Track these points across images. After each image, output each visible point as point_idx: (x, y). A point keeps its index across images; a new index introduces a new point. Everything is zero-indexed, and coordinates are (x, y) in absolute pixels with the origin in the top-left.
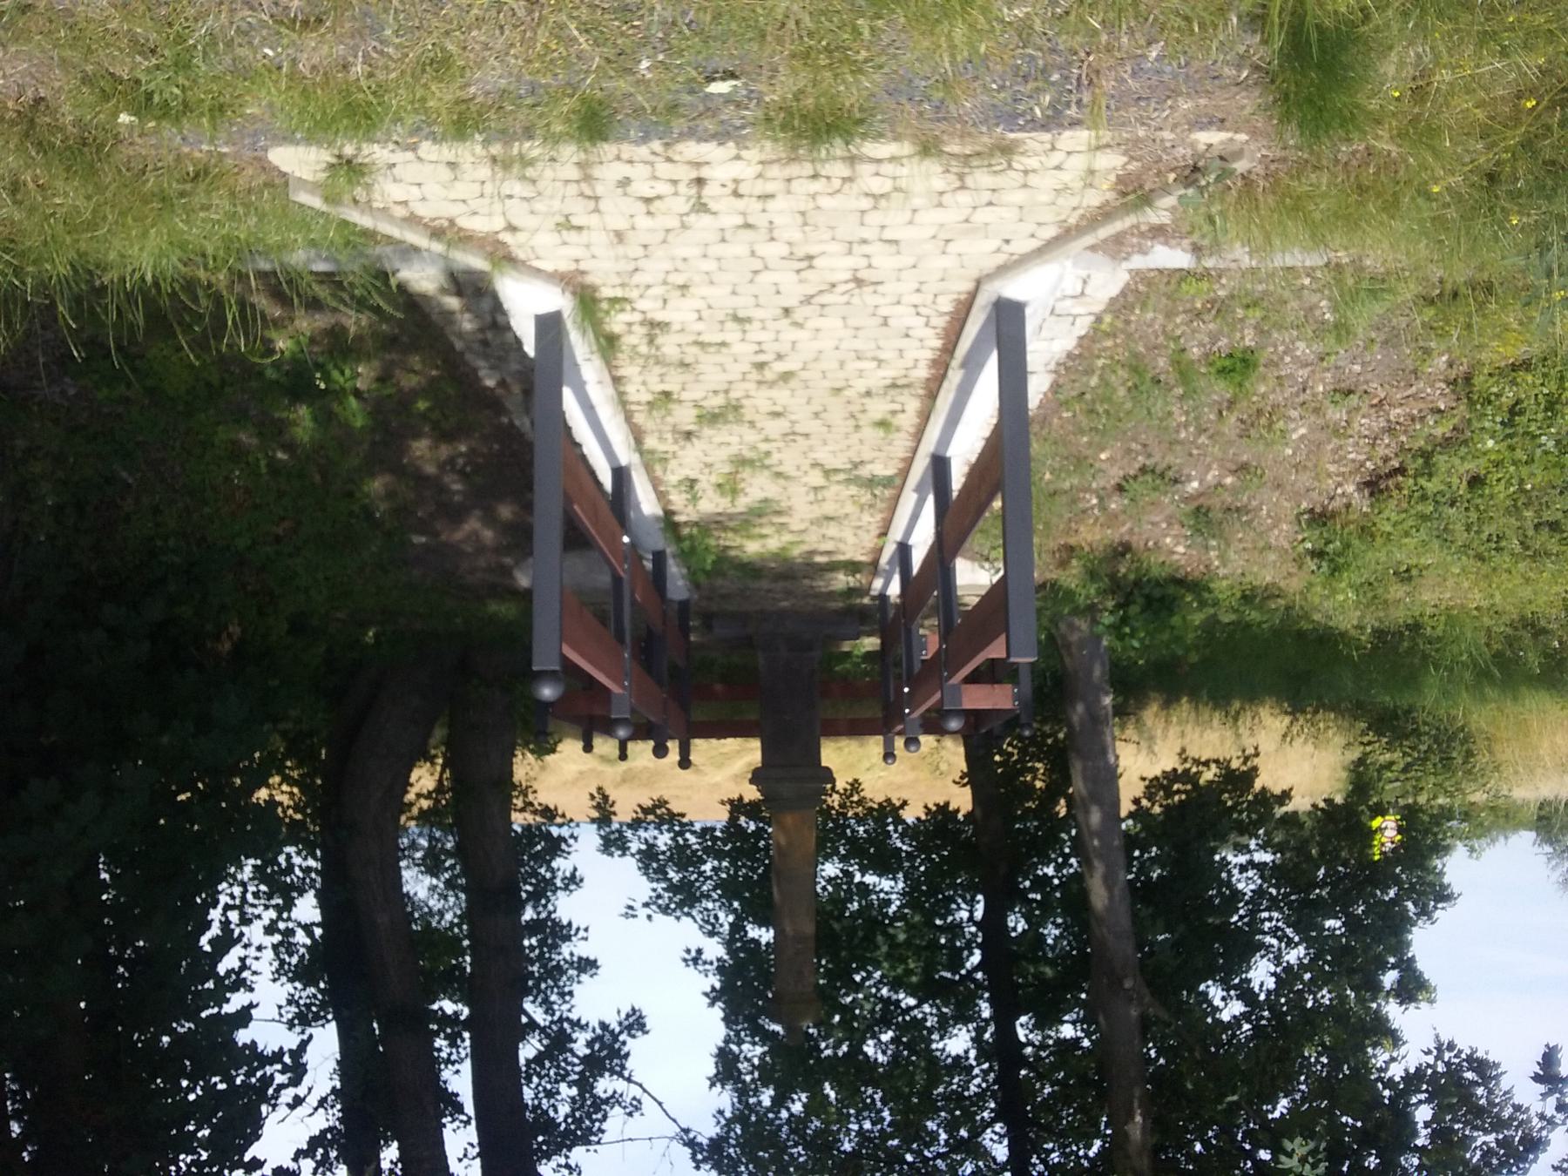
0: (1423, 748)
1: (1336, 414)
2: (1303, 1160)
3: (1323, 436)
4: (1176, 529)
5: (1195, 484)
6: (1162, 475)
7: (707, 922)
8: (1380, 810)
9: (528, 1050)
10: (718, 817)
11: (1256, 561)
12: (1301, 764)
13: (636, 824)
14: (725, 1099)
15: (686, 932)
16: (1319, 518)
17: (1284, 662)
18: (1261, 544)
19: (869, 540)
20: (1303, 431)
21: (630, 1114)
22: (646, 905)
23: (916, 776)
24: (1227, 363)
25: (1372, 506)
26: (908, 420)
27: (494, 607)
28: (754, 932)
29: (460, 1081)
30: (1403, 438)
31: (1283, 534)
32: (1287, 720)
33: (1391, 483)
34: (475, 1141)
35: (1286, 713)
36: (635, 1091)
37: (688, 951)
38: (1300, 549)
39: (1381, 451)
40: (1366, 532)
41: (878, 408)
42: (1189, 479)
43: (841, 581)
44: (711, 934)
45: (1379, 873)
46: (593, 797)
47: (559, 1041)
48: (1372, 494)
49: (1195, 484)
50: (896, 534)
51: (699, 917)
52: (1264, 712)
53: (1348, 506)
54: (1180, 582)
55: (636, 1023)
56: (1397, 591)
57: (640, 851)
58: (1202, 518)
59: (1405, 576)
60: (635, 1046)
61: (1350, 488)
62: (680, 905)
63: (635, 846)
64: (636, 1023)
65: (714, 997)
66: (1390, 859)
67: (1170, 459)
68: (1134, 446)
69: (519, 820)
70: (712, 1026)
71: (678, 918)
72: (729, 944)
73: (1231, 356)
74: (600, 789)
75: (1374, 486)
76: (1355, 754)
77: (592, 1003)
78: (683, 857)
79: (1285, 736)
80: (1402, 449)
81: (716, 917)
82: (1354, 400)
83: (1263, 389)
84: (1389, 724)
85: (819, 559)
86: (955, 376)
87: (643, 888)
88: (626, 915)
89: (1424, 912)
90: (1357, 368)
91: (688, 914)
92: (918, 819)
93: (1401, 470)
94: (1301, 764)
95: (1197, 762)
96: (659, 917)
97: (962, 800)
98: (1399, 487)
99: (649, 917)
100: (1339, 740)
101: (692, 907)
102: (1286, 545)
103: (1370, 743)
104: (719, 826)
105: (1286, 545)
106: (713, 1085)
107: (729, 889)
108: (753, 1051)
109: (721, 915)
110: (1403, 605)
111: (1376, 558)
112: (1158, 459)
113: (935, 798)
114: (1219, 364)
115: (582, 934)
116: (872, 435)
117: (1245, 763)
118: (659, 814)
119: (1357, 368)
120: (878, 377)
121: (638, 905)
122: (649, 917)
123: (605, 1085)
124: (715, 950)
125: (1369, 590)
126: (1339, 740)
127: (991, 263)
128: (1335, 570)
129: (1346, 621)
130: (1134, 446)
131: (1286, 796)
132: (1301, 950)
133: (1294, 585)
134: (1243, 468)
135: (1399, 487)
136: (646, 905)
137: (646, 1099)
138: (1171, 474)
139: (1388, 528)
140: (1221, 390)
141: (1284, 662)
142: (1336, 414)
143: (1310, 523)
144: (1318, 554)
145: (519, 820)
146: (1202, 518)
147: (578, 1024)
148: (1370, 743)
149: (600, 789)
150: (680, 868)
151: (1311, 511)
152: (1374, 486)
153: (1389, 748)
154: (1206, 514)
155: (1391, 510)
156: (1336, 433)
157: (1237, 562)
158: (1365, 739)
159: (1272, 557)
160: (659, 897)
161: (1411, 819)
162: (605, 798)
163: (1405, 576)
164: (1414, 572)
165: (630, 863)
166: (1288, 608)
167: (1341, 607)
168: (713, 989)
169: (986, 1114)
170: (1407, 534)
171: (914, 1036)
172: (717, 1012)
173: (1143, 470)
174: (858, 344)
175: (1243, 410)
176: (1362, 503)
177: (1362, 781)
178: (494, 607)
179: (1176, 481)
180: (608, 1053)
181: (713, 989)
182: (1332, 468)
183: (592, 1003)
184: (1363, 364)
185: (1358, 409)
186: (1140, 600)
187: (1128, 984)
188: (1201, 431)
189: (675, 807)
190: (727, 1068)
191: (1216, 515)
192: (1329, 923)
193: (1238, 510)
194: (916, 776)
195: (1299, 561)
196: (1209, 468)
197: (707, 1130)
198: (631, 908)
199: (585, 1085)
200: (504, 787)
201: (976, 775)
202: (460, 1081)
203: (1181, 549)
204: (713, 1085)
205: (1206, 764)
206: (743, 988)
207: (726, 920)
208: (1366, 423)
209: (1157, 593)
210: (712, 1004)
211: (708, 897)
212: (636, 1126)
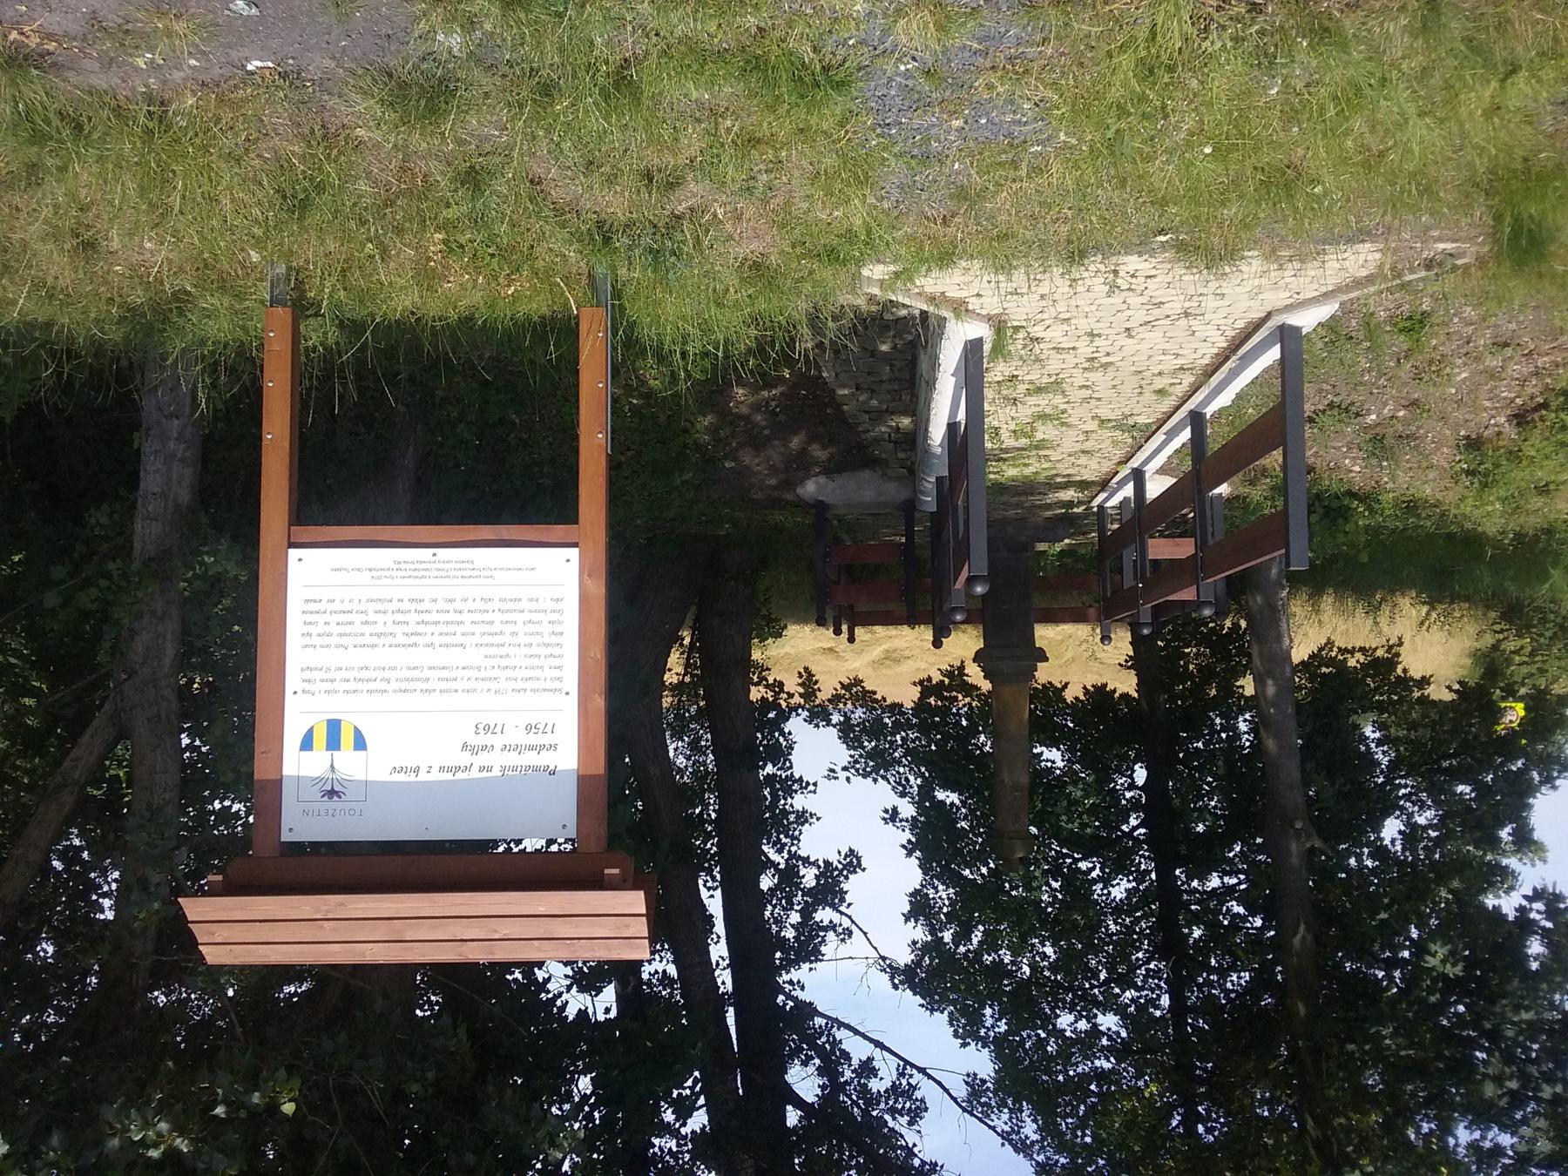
0: (1548, 634)
1: (1493, 362)
2: (1444, 962)
3: (1483, 378)
4: (1355, 453)
5: (1374, 417)
6: (1347, 410)
7: (899, 783)
8: (1510, 692)
9: (766, 882)
10: (908, 696)
11: (1425, 478)
12: (1435, 650)
13: (836, 699)
14: (920, 933)
15: (881, 794)
16: (1473, 444)
17: (1435, 562)
18: (1424, 464)
19: (1107, 466)
20: (1464, 375)
21: (843, 940)
22: (845, 769)
23: (1084, 658)
24: (1408, 324)
25: (1519, 434)
26: (1180, 390)
27: (778, 517)
28: (940, 795)
29: (714, 904)
30: (1548, 380)
31: (1444, 456)
32: (1425, 609)
33: (1536, 416)
34: (726, 954)
35: (1424, 603)
36: (846, 923)
37: (886, 811)
38: (1457, 468)
39: (1529, 390)
40: (1515, 455)
41: (1160, 383)
42: (1369, 412)
43: (1069, 495)
44: (903, 795)
45: (1508, 745)
46: (800, 676)
47: (789, 876)
48: (1519, 424)
49: (1374, 417)
50: (1135, 463)
51: (892, 780)
52: (1405, 602)
53: (1499, 434)
54: (1351, 494)
55: (853, 862)
56: (1537, 502)
57: (840, 723)
58: (1378, 445)
59: (1544, 490)
60: (853, 886)
61: (1503, 420)
62: (876, 770)
63: (835, 718)
64: (853, 862)
65: (909, 850)
66: (1513, 734)
67: (1354, 397)
68: (1325, 386)
69: (756, 693)
70: (910, 874)
71: (875, 780)
72: (919, 806)
73: (1410, 318)
74: (806, 669)
75: (1521, 418)
76: (1489, 640)
77: (818, 844)
78: (875, 729)
79: (1422, 623)
80: (1547, 388)
81: (907, 780)
82: (1508, 352)
83: (1434, 342)
84: (1514, 614)
85: (1059, 480)
86: (1230, 364)
87: (842, 755)
88: (828, 777)
89: (1548, 780)
90: (1513, 326)
91: (884, 778)
92: (1077, 698)
93: (1545, 406)
94: (1435, 650)
95: (1346, 651)
96: (857, 780)
97: (1126, 684)
98: (1542, 419)
99: (848, 779)
100: (1472, 629)
101: (886, 770)
102: (1446, 465)
103: (1502, 631)
104: (800, 719)
105: (1446, 465)
106: (907, 920)
107: (916, 757)
108: (943, 894)
109: (911, 778)
110: (1538, 514)
111: (1520, 476)
112: (1343, 398)
113: (1091, 680)
114: (1401, 325)
115: (811, 788)
116: (1149, 396)
117: (1388, 651)
118: (855, 691)
119: (1513, 326)
120: (1171, 363)
121: (838, 769)
122: (848, 779)
123: (824, 915)
124: (907, 810)
125: (1514, 504)
126: (1472, 629)
127: (1280, 304)
128: (1485, 485)
129: (1491, 528)
130: (1325, 386)
131: (1424, 682)
132: (1430, 814)
133: (1451, 497)
134: (1414, 403)
135: (1542, 419)
136: (845, 769)
137: (854, 928)
138: (1354, 409)
139: (1533, 453)
140: (1402, 342)
141: (1435, 562)
142: (1493, 362)
143: (1467, 447)
144: (1469, 473)
145: (756, 693)
146: (1378, 445)
147: (806, 861)
148: (1502, 631)
149: (806, 669)
150: (874, 735)
151: (1467, 438)
152: (1521, 418)
153: (1520, 635)
154: (1381, 441)
155: (1536, 437)
156: (1492, 377)
157: (1403, 478)
158: (1497, 627)
159: (1432, 475)
160: (856, 762)
161: (1538, 703)
162: (810, 675)
163: (1544, 490)
164: (1552, 487)
165: (833, 732)
166: (1443, 514)
167: (1490, 516)
168: (909, 841)
169: (1140, 955)
170: (1547, 457)
171: (1077, 886)
172: (913, 862)
173: (1331, 405)
174: (1167, 346)
175: (1418, 359)
176: (1511, 432)
177: (1491, 666)
178: (778, 517)
179: (1357, 415)
180: (830, 889)
181: (909, 841)
182: (1487, 404)
183: (818, 844)
184: (1518, 323)
185: (1511, 358)
186: (1321, 511)
187: (1298, 825)
188: (1381, 374)
189: (868, 686)
190: (920, 907)
191: (1388, 441)
192: (1460, 788)
193: (1408, 437)
194: (1084, 658)
195: (1455, 479)
196: (1385, 404)
197: (904, 957)
198: (832, 770)
199: (807, 913)
200: (745, 669)
201: (1137, 663)
202: (714, 904)
203: (1357, 468)
204: (907, 920)
205: (1352, 652)
206: (933, 840)
207: (915, 782)
208: (1518, 368)
209: (1335, 504)
210: (909, 854)
211: (899, 763)
212: (846, 949)
